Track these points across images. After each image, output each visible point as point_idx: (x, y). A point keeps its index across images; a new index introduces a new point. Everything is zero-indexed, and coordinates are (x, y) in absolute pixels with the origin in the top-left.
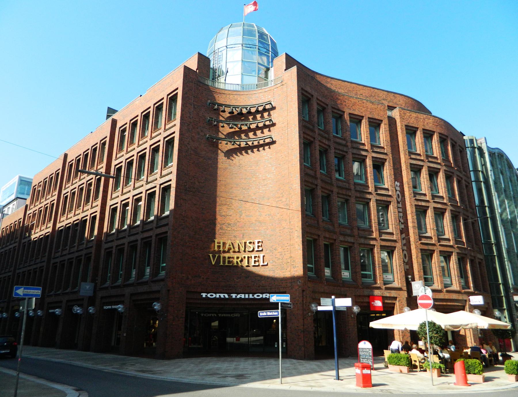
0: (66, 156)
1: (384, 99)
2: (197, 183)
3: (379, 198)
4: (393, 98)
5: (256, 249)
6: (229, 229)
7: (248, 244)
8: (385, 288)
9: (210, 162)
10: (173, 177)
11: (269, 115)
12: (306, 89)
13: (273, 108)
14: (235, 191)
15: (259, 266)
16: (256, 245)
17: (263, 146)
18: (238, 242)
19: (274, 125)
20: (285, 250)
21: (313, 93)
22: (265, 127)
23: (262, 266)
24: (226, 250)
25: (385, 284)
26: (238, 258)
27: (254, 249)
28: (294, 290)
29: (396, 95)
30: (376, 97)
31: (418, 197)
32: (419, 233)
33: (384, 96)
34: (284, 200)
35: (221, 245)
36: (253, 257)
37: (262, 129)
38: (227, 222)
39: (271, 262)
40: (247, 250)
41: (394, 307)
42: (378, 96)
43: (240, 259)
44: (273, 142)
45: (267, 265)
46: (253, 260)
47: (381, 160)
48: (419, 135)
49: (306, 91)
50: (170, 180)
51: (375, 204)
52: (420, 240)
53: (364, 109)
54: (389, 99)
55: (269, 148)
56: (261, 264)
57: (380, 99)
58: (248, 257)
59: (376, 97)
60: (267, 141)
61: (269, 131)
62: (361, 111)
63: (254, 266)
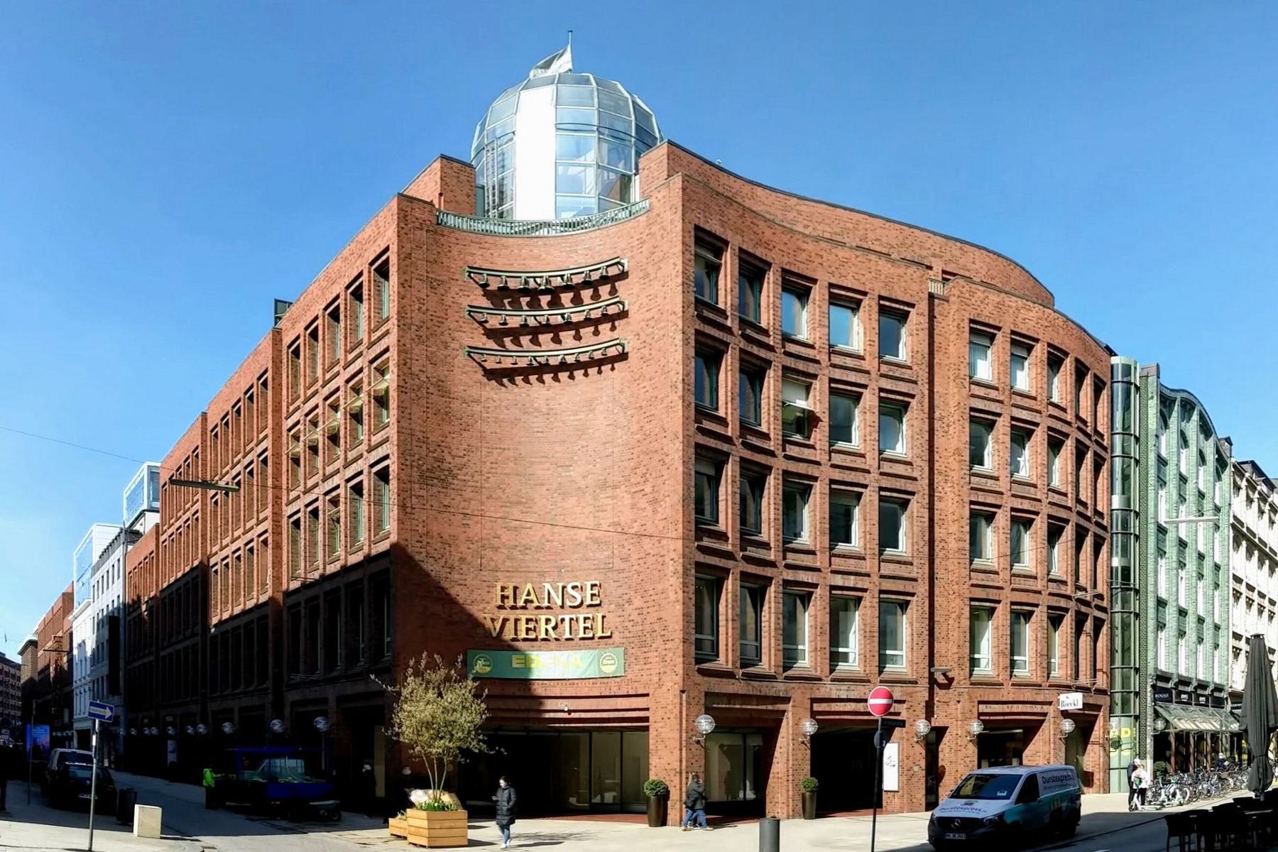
0: (204, 416)
1: (934, 256)
2: (449, 459)
3: (748, 454)
4: (958, 253)
5: (588, 602)
6: (527, 558)
7: (569, 589)
8: (744, 674)
9: (477, 408)
10: (390, 449)
11: (613, 292)
12: (707, 227)
13: (623, 275)
14: (540, 473)
15: (536, 640)
16: (589, 592)
17: (599, 363)
18: (529, 586)
19: (623, 315)
20: (650, 604)
21: (729, 236)
22: (606, 318)
23: (601, 638)
24: (521, 603)
25: (743, 666)
26: (548, 621)
27: (582, 603)
28: (665, 689)
29: (967, 248)
30: (916, 248)
31: (707, 425)
32: (697, 522)
33: (937, 247)
34: (648, 489)
35: (509, 592)
36: (581, 620)
37: (595, 323)
38: (524, 542)
39: (620, 629)
40: (568, 603)
41: (781, 721)
42: (921, 247)
43: (553, 624)
44: (623, 356)
45: (610, 637)
46: (582, 625)
47: (758, 362)
48: (729, 263)
49: (710, 234)
50: (386, 457)
51: (737, 469)
52: (698, 538)
53: (869, 276)
54: (947, 256)
55: (613, 369)
56: (600, 634)
57: (924, 253)
58: (571, 619)
59: (916, 248)
60: (612, 352)
61: (613, 328)
62: (863, 280)
63: (525, 640)
